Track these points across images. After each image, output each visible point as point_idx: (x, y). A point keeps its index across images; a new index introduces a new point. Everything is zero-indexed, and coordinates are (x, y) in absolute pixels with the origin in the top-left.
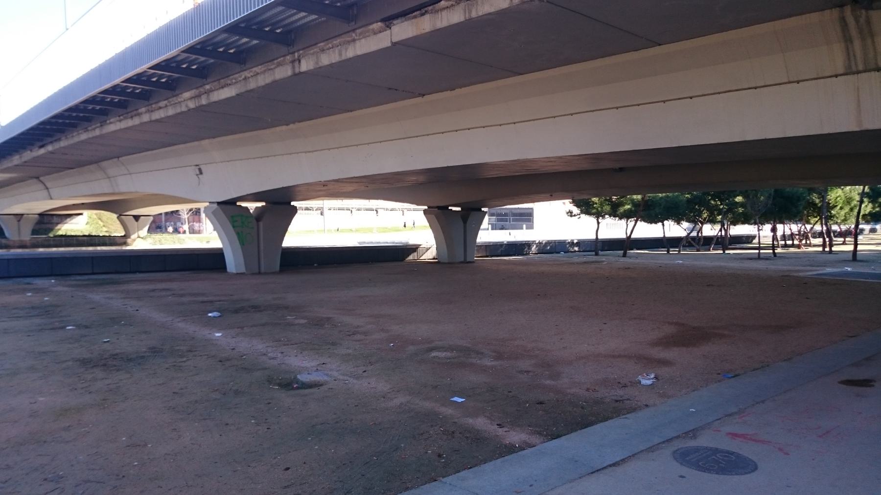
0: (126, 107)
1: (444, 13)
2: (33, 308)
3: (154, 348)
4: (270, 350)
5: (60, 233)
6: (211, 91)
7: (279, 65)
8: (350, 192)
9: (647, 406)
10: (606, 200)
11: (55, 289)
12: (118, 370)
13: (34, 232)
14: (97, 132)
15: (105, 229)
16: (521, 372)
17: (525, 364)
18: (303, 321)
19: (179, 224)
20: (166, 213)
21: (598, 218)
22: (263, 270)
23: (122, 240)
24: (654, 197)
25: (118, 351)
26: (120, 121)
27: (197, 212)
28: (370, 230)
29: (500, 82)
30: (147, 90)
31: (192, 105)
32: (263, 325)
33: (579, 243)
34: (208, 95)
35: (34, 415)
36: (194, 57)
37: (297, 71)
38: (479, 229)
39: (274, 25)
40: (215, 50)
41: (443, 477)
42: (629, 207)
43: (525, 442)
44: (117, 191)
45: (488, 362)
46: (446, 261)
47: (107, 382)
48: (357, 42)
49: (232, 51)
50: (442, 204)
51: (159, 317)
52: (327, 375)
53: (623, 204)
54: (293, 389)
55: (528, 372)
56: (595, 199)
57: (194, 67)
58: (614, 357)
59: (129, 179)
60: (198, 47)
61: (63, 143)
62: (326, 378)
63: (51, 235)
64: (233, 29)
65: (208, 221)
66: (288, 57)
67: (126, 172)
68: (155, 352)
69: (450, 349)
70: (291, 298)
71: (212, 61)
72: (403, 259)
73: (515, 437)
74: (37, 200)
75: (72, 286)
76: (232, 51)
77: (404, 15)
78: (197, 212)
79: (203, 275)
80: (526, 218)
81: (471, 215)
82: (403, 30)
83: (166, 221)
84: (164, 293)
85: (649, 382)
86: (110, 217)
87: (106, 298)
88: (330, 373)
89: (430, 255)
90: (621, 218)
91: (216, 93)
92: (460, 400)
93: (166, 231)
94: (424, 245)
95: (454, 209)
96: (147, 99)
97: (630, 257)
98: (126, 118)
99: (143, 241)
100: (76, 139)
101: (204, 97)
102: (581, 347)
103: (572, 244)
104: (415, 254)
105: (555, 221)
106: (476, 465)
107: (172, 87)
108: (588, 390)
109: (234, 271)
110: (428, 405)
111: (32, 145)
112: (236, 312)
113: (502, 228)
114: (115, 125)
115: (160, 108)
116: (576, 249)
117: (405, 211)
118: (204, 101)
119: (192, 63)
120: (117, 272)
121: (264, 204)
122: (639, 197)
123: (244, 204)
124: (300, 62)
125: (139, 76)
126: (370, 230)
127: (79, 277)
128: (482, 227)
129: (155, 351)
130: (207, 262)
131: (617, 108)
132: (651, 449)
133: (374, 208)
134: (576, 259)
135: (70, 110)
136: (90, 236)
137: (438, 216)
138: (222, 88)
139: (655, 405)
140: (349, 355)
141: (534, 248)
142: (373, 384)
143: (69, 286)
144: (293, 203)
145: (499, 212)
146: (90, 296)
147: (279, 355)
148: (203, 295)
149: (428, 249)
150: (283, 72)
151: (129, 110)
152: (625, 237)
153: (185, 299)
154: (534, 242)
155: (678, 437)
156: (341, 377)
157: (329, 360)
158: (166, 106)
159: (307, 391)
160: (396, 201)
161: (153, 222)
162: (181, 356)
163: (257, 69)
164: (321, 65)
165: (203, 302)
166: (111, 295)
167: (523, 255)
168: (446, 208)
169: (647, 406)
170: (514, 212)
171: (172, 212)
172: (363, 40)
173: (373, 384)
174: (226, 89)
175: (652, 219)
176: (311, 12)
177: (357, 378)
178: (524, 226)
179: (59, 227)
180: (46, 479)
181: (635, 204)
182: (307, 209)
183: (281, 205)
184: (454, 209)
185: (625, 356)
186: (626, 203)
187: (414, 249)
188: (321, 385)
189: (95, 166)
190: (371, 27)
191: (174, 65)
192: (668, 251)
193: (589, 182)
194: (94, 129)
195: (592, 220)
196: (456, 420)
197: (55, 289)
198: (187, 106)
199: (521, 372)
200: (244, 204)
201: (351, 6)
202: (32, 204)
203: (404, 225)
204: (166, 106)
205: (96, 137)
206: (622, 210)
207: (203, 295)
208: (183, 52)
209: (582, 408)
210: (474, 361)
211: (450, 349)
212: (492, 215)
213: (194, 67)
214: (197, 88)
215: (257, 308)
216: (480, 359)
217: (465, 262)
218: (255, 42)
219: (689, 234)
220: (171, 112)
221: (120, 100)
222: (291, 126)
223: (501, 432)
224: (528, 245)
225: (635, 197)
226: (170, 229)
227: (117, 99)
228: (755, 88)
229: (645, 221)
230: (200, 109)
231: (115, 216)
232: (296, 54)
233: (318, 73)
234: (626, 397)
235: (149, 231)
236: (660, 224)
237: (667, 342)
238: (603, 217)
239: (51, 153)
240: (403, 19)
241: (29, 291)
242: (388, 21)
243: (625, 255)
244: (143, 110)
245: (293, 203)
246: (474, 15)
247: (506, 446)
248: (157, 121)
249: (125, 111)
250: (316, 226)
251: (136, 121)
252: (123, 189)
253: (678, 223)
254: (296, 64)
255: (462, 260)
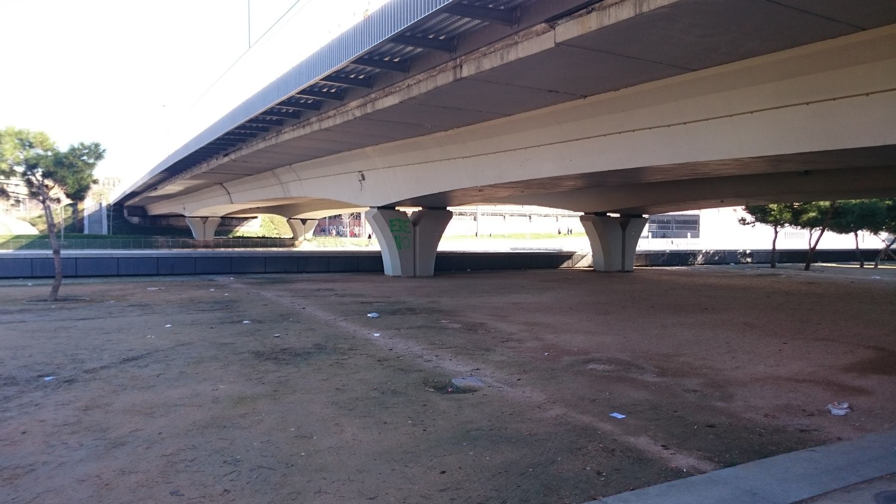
0: (298, 118)
1: (612, 10)
2: (215, 302)
3: (318, 345)
4: (425, 352)
5: (238, 234)
6: (376, 99)
7: (441, 71)
8: (505, 197)
9: (839, 439)
10: (786, 207)
11: (234, 286)
12: (287, 364)
13: (217, 233)
14: (273, 141)
15: (276, 232)
16: (688, 391)
17: (692, 383)
18: (456, 326)
19: (341, 228)
20: (330, 218)
21: (776, 226)
22: (418, 274)
23: (290, 242)
24: (845, 204)
25: (287, 346)
26: (293, 130)
27: (358, 216)
28: (523, 236)
29: (842, 41)
30: (318, 101)
31: (358, 113)
32: (419, 327)
33: (753, 254)
34: (373, 104)
35: (216, 400)
36: (362, 67)
37: (458, 76)
38: (639, 236)
39: (438, 32)
40: (381, 60)
41: (604, 496)
42: (814, 214)
43: (694, 467)
44: (288, 196)
45: (650, 378)
46: (603, 269)
47: (279, 374)
48: (520, 45)
49: (396, 60)
50: (600, 210)
51: (322, 315)
52: (481, 381)
53: (806, 212)
54: (448, 392)
55: (695, 391)
56: (774, 206)
57: (361, 77)
58: (797, 381)
59: (300, 185)
60: (366, 57)
61: (244, 152)
62: (480, 384)
63: (231, 236)
64: (399, 38)
65: (368, 225)
66: (450, 63)
67: (297, 178)
68: (320, 348)
69: (609, 361)
70: (446, 302)
71: (378, 70)
72: (557, 267)
73: (683, 460)
74: (220, 204)
75: (249, 283)
76: (396, 60)
77: (569, 14)
78: (358, 216)
79: (362, 277)
80: (692, 225)
81: (631, 222)
82: (568, 30)
83: (330, 225)
84: (328, 293)
85: (842, 412)
86: (281, 220)
87: (276, 295)
88: (484, 379)
89: (585, 263)
90: (803, 227)
91: (380, 101)
92: (620, 416)
93: (330, 234)
94: (580, 252)
95: (613, 215)
96: (318, 109)
97: (814, 271)
98: (298, 128)
99: (309, 243)
100: (255, 148)
101: (369, 106)
102: (759, 370)
103: (744, 254)
104: (570, 261)
105: (725, 229)
106: (639, 488)
107: (340, 97)
108: (766, 416)
109: (391, 274)
110: (586, 419)
111: (218, 153)
112: (393, 313)
113: (664, 237)
114: (289, 134)
115: (329, 117)
116: (749, 260)
117: (559, 217)
118: (369, 109)
119: (359, 73)
120: (286, 272)
121: (421, 209)
122: (827, 203)
123: (402, 209)
124: (461, 67)
125: (312, 87)
126: (523, 236)
127: (255, 276)
128: (642, 235)
129: (320, 348)
130: (368, 264)
131: (808, 104)
132: (846, 489)
133: (528, 214)
134: (749, 272)
135: (238, 128)
136: (263, 237)
137: (595, 222)
138: (387, 96)
139: (849, 439)
140: (503, 361)
141: (700, 258)
142: (529, 393)
143: (244, 283)
144: (448, 208)
145: (661, 219)
146: (263, 293)
147: (434, 358)
148: (362, 296)
149: (583, 257)
150: (445, 78)
151: (301, 120)
152: (807, 247)
153: (345, 300)
154: (700, 252)
155: (881, 478)
156: (496, 384)
157: (483, 366)
158: (335, 115)
159: (462, 396)
160: (550, 207)
161: (318, 225)
162: (343, 354)
163: (420, 77)
164: (482, 69)
165: (363, 303)
166: (281, 293)
167: (688, 265)
168: (604, 214)
169: (839, 439)
170: (677, 219)
171: (335, 216)
172: (526, 43)
173: (529, 393)
174: (390, 97)
175: (842, 229)
176: (474, 18)
177: (512, 386)
178: (689, 234)
179: (237, 229)
180: (225, 462)
181: (822, 211)
182: (461, 214)
183: (437, 209)
184: (613, 215)
185: (810, 381)
186: (811, 211)
187: (569, 256)
188: (476, 391)
189: (270, 172)
190: (534, 29)
191: (343, 75)
192: (862, 266)
193: (763, 188)
194: (271, 139)
195: (768, 229)
196: (616, 438)
197: (234, 286)
198: (353, 114)
199: (688, 391)
200: (402, 209)
201: (515, 8)
202: (216, 207)
203: (562, 232)
204: (335, 115)
205: (273, 146)
206: (805, 217)
207: (362, 296)
208: (353, 62)
209: (760, 435)
210: (634, 376)
211: (609, 361)
212: (653, 222)
213: (361, 77)
214: (363, 97)
215: (412, 311)
216: (641, 374)
217: (623, 271)
218: (419, 50)
219: (888, 246)
220: (338, 121)
221: (294, 111)
222: (450, 132)
223: (666, 453)
224: (693, 254)
225: (822, 203)
226: (334, 232)
227: (291, 109)
228: (834, 99)
229: (833, 230)
230: (366, 117)
231: (285, 219)
232: (458, 60)
233: (479, 78)
234: (814, 427)
235: (315, 234)
236: (852, 234)
237: (863, 368)
238: (782, 226)
239: (234, 161)
240: (568, 18)
241: (212, 286)
242: (552, 22)
243: (807, 268)
244: (314, 119)
245: (448, 208)
246: (645, 9)
247: (672, 469)
248: (326, 129)
249: (297, 121)
250: (472, 231)
251: (308, 130)
252: (294, 194)
253: (876, 234)
254: (458, 70)
255: (620, 268)
